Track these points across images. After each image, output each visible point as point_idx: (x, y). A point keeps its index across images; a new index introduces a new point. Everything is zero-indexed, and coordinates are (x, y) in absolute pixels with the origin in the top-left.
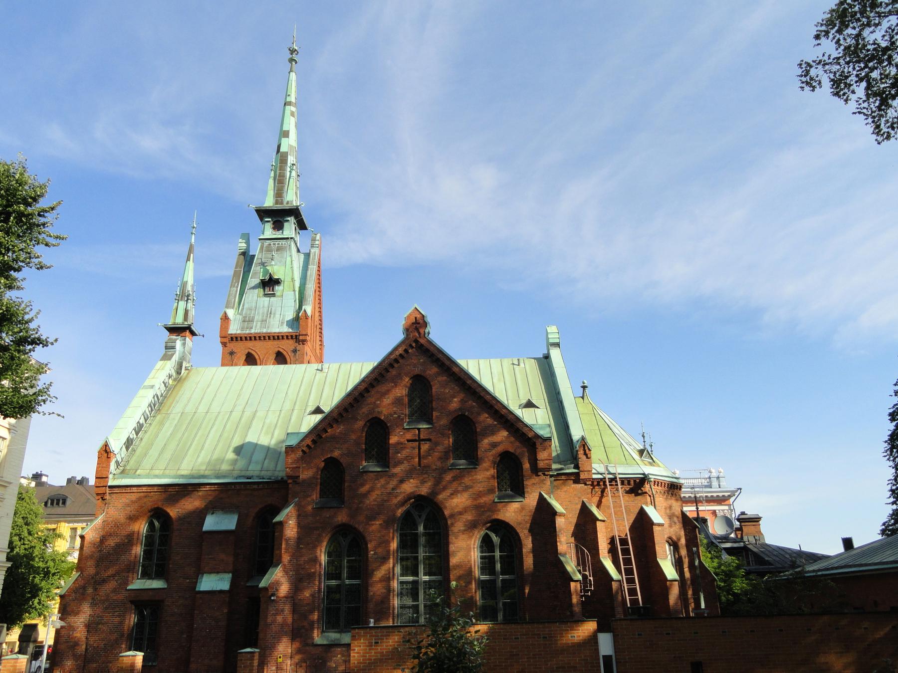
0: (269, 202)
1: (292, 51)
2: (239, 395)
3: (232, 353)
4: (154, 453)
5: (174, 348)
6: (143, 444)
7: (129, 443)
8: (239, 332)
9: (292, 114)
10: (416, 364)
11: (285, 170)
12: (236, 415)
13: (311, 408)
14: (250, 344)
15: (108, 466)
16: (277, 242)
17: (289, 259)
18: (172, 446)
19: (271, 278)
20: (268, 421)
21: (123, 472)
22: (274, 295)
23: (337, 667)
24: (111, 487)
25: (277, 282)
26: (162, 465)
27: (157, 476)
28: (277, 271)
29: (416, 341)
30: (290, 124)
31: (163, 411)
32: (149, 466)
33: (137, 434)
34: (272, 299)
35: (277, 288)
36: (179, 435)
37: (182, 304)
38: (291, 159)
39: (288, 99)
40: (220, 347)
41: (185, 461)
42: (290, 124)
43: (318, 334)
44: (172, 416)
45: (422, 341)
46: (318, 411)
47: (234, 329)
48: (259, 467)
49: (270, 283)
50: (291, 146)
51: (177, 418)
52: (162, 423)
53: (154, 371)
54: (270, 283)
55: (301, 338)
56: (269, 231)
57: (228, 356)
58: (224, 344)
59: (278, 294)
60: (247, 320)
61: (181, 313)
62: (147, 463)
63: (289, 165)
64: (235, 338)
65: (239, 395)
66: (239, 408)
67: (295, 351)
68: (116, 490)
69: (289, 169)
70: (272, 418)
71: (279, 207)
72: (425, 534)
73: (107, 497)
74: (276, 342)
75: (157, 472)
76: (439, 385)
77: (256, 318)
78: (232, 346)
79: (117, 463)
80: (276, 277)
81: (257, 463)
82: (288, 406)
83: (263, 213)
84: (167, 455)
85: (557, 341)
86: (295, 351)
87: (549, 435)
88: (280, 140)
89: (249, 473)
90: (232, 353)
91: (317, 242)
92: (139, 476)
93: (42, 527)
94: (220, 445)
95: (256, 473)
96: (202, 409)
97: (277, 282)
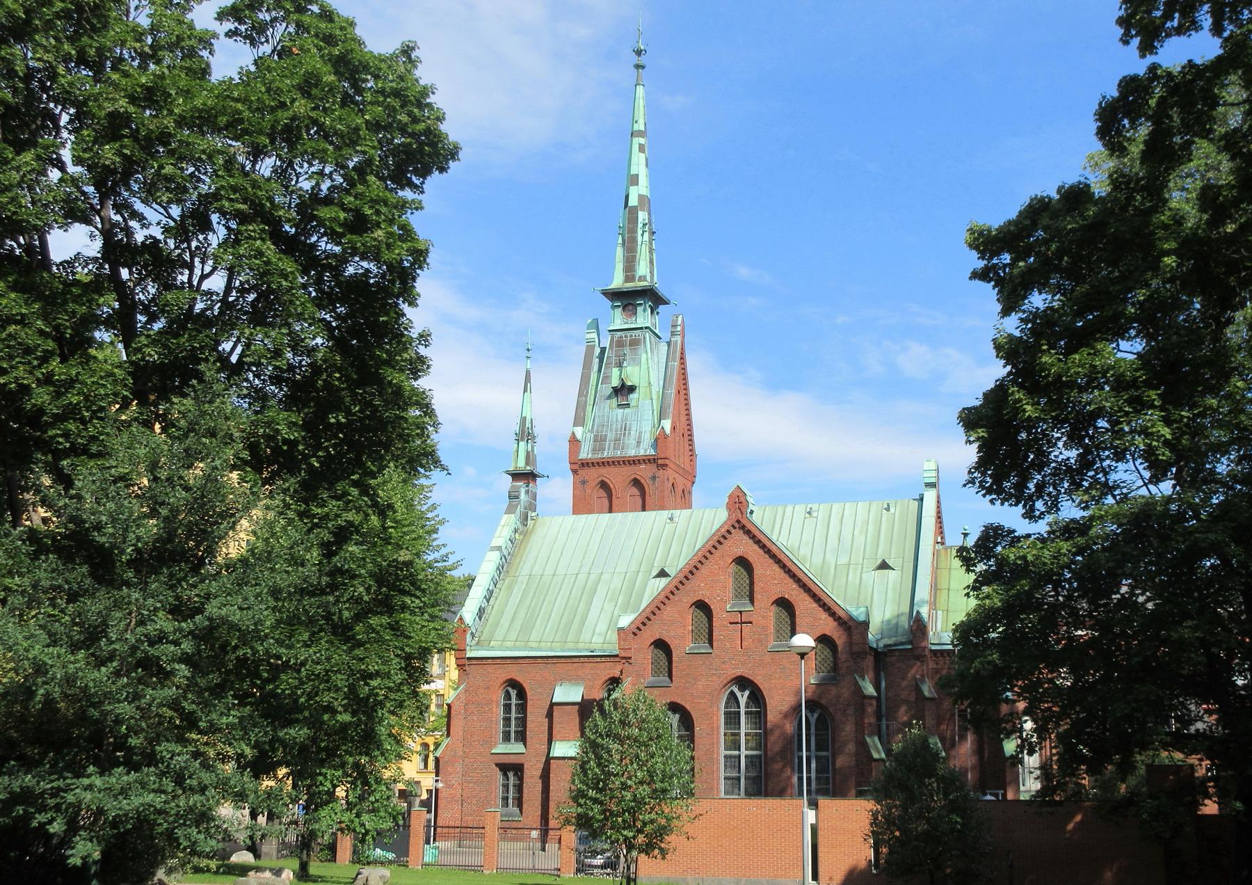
0: (618, 281)
3: (584, 482)
4: (505, 622)
7: (481, 612)
9: (642, 148)
12: (582, 577)
13: (655, 572)
16: (629, 333)
17: (644, 356)
18: (522, 614)
19: (623, 385)
21: (477, 644)
22: (628, 405)
24: (469, 659)
25: (632, 389)
27: (508, 649)
28: (633, 374)
29: (738, 522)
30: (639, 164)
31: (512, 573)
32: (501, 638)
39: (636, 127)
40: (571, 476)
42: (639, 164)
45: (744, 522)
47: (585, 453)
49: (624, 390)
52: (510, 588)
54: (624, 390)
57: (579, 485)
58: (575, 472)
59: (633, 404)
60: (599, 440)
61: (522, 455)
62: (499, 634)
63: (640, 225)
64: (585, 464)
66: (586, 569)
67: (654, 478)
68: (474, 662)
69: (640, 232)
71: (630, 286)
72: (1123, 595)
73: (467, 668)
77: (609, 435)
79: (473, 635)
82: (633, 568)
85: (933, 480)
86: (654, 478)
87: (862, 618)
90: (584, 482)
91: (679, 328)
92: (493, 649)
97: (632, 389)
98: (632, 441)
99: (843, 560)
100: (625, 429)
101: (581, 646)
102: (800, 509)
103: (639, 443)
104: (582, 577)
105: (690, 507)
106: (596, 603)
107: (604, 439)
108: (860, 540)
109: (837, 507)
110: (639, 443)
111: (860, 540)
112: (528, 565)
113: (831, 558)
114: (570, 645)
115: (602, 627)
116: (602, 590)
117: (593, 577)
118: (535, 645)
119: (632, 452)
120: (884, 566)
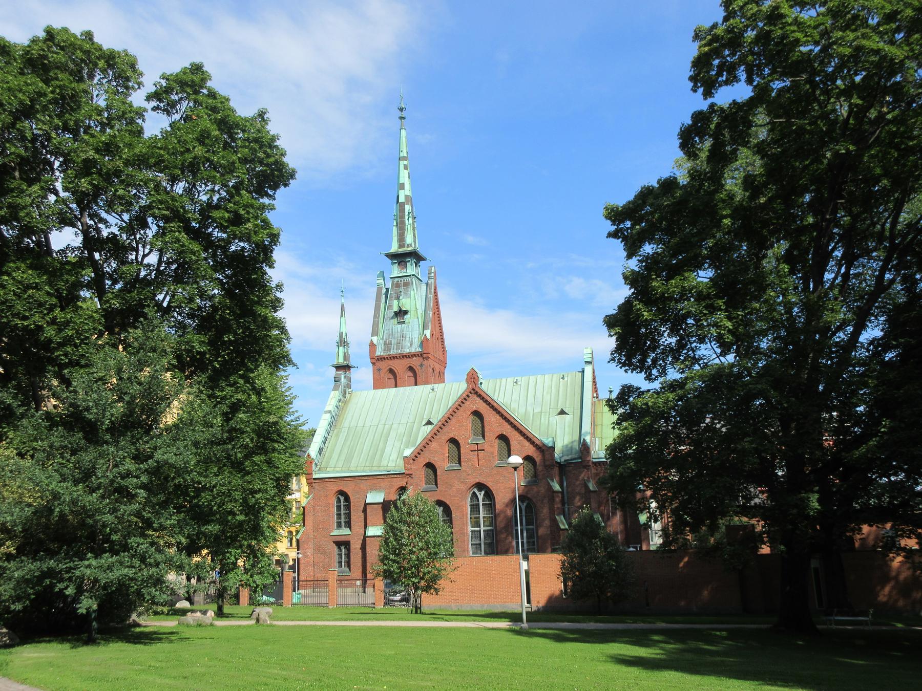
0: (394, 248)
1: (401, 110)
3: (379, 370)
4: (335, 456)
7: (320, 451)
9: (405, 167)
10: (476, 404)
13: (424, 422)
16: (402, 279)
18: (345, 451)
22: (404, 322)
23: (76, 599)
25: (406, 312)
27: (338, 472)
28: (406, 303)
30: (404, 177)
37: (341, 348)
38: (408, 208)
42: (404, 177)
45: (477, 389)
47: (379, 352)
48: (393, 464)
50: (406, 197)
52: (338, 435)
54: (401, 313)
58: (373, 364)
59: (407, 321)
60: (387, 344)
62: (332, 463)
64: (380, 359)
66: (382, 422)
67: (421, 365)
71: (402, 250)
74: (409, 360)
75: (338, 469)
76: (490, 418)
78: (379, 364)
82: (411, 420)
84: (343, 457)
86: (421, 365)
89: (389, 468)
92: (328, 472)
93: (282, 547)
96: (360, 424)
97: (406, 312)
99: (538, 410)
100: (403, 337)
101: (382, 468)
102: (510, 380)
103: (411, 345)
105: (444, 382)
106: (390, 443)
107: (390, 343)
108: (547, 397)
109: (532, 378)
110: (411, 345)
111: (547, 397)
112: (347, 421)
113: (530, 409)
114: (375, 468)
115: (394, 456)
116: (393, 434)
118: (354, 469)
119: (407, 351)
120: (562, 412)
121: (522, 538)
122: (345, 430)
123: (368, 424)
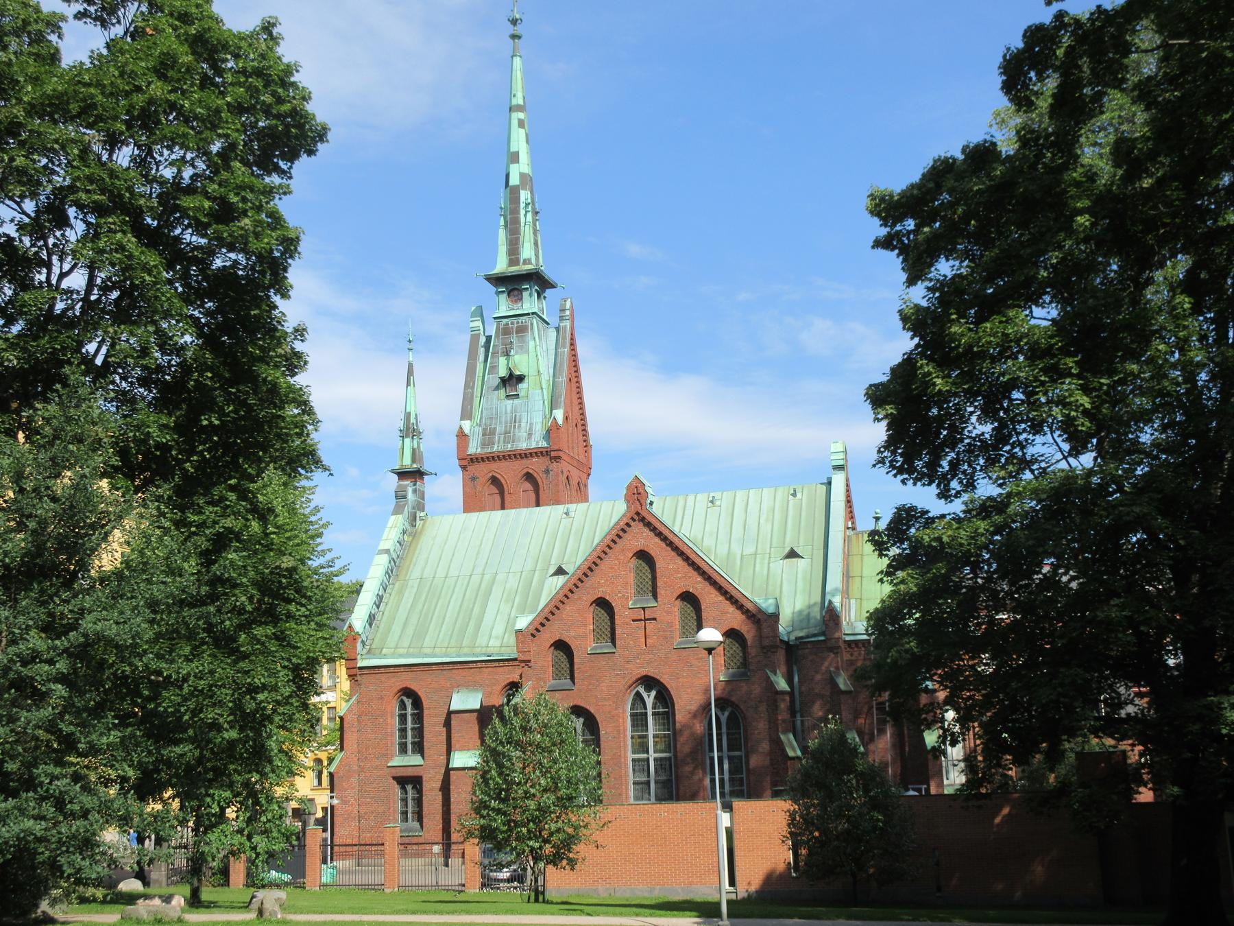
0: (501, 266)
1: (514, 22)
2: (478, 553)
3: (473, 479)
4: (397, 628)
5: (405, 497)
6: (385, 618)
7: (371, 619)
8: (479, 451)
9: (521, 124)
10: (642, 539)
11: (518, 212)
12: (476, 579)
14: (494, 466)
15: (355, 648)
16: (515, 320)
18: (414, 620)
19: (511, 375)
20: (508, 586)
21: (369, 652)
24: (361, 668)
25: (520, 379)
26: (406, 643)
28: (521, 363)
29: (638, 514)
30: (519, 141)
31: (401, 577)
32: (393, 645)
33: (378, 607)
34: (516, 401)
35: (520, 386)
36: (420, 606)
37: (407, 441)
39: (514, 102)
41: (427, 639)
42: (519, 141)
43: (581, 434)
44: (410, 583)
45: (644, 514)
46: (560, 571)
47: (474, 448)
48: (498, 644)
50: (522, 176)
51: (416, 586)
52: (401, 592)
53: (387, 530)
54: (512, 380)
55: (553, 454)
56: (504, 307)
58: (464, 468)
59: (522, 394)
60: (488, 434)
62: (392, 640)
63: (522, 205)
64: (474, 460)
65: (478, 553)
66: (479, 570)
67: (547, 471)
70: (512, 583)
71: (514, 269)
72: (1044, 575)
75: (401, 651)
76: (667, 563)
78: (475, 468)
80: (518, 373)
81: (497, 638)
83: (499, 281)
84: (410, 631)
85: (841, 462)
86: (547, 471)
87: (771, 610)
88: (508, 167)
89: (490, 650)
91: (568, 313)
92: (385, 656)
94: (461, 617)
95: (496, 650)
96: (441, 573)
97: (520, 379)
98: (523, 434)
104: (476, 579)
114: (466, 650)
116: (497, 592)
117: (487, 577)
119: (523, 445)
121: (720, 772)
122: (413, 583)
123: (454, 572)
